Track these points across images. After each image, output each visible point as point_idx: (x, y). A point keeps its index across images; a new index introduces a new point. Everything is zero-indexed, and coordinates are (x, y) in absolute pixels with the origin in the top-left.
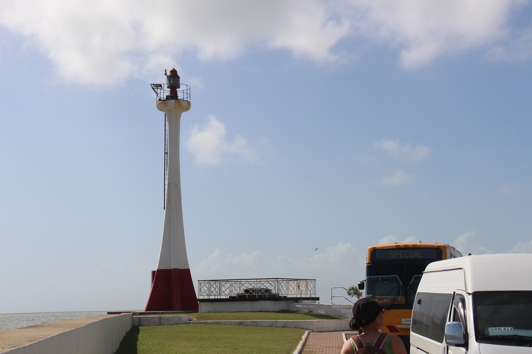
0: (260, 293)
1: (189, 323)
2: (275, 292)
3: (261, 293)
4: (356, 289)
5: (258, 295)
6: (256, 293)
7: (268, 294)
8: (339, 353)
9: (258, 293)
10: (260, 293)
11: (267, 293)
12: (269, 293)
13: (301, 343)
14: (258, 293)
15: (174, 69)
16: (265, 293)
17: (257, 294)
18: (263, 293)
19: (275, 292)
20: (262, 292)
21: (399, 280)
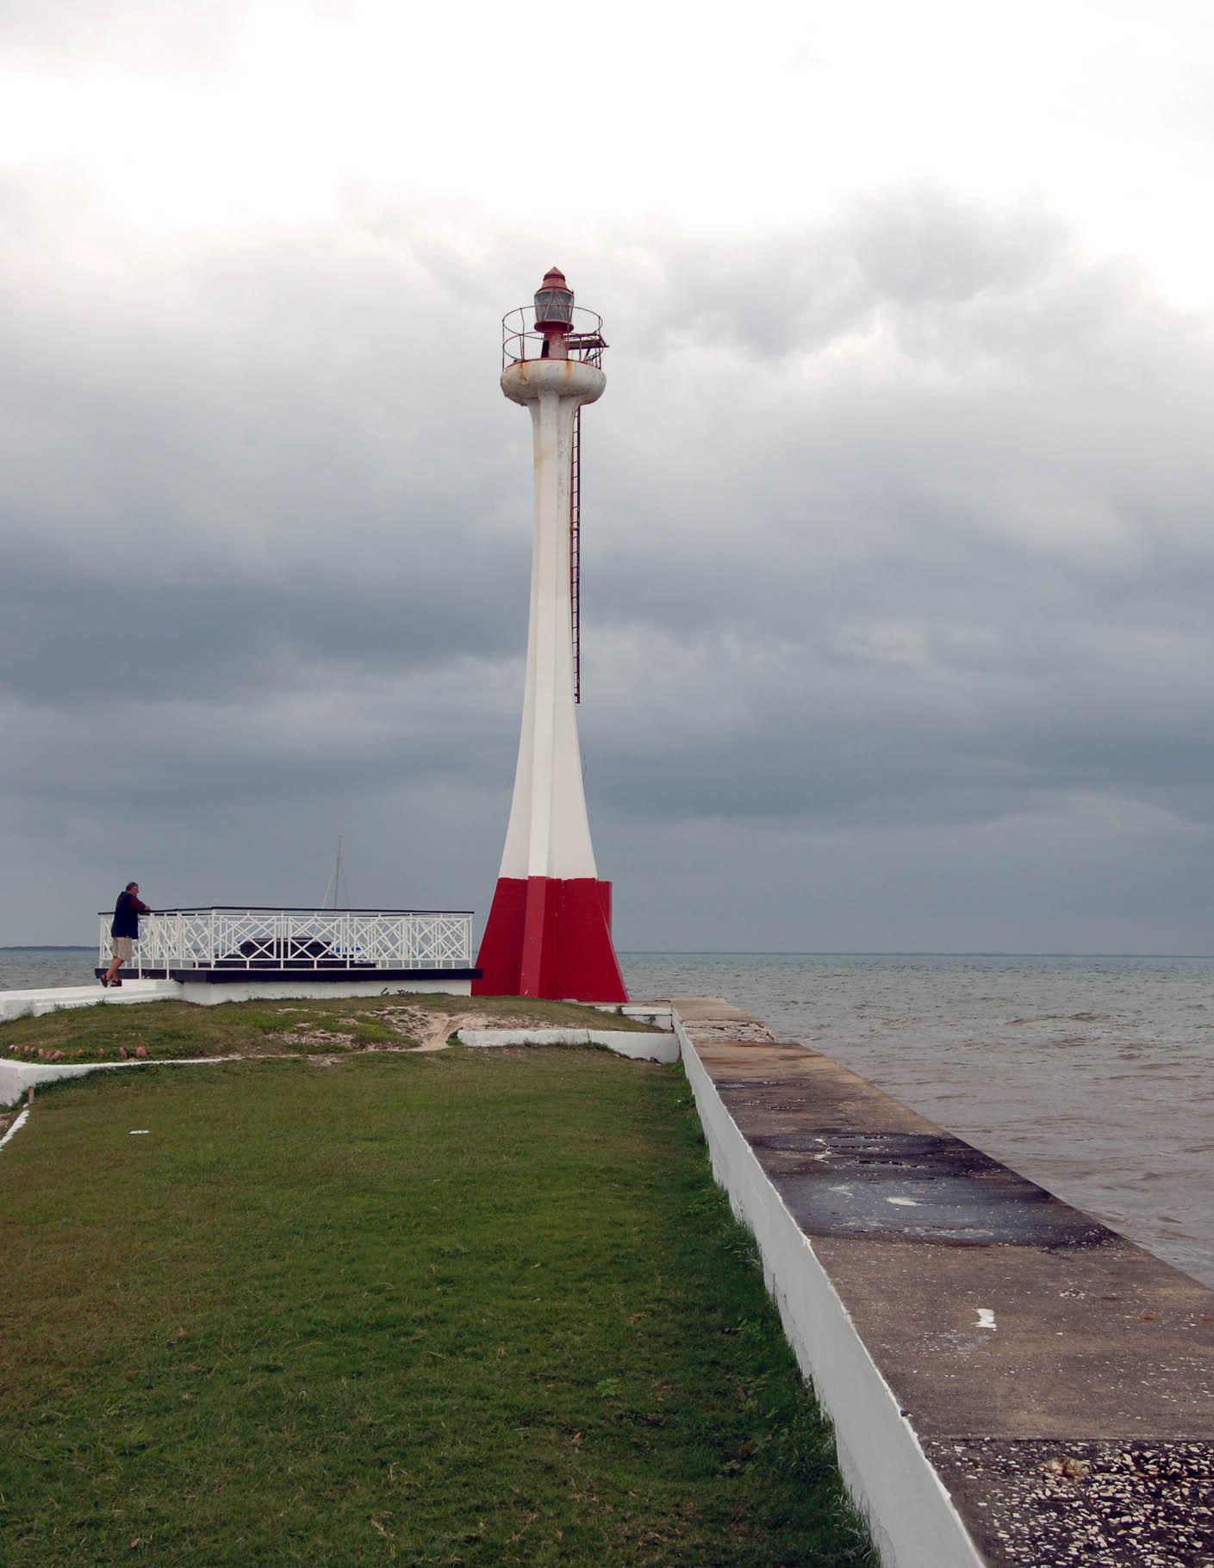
0: (292, 954)
1: (1174, 1234)
2: (439, 966)
3: (294, 955)
4: (1181, 1322)
5: (285, 961)
6: (279, 956)
7: (250, 959)
8: (7, 1055)
9: (286, 956)
10: (292, 954)
11: (248, 956)
12: (322, 954)
13: (81, 1068)
14: (286, 956)
15: (555, 268)
16: (243, 956)
17: (282, 959)
18: (302, 955)
19: (439, 966)
20: (299, 951)
21: (195, 1061)
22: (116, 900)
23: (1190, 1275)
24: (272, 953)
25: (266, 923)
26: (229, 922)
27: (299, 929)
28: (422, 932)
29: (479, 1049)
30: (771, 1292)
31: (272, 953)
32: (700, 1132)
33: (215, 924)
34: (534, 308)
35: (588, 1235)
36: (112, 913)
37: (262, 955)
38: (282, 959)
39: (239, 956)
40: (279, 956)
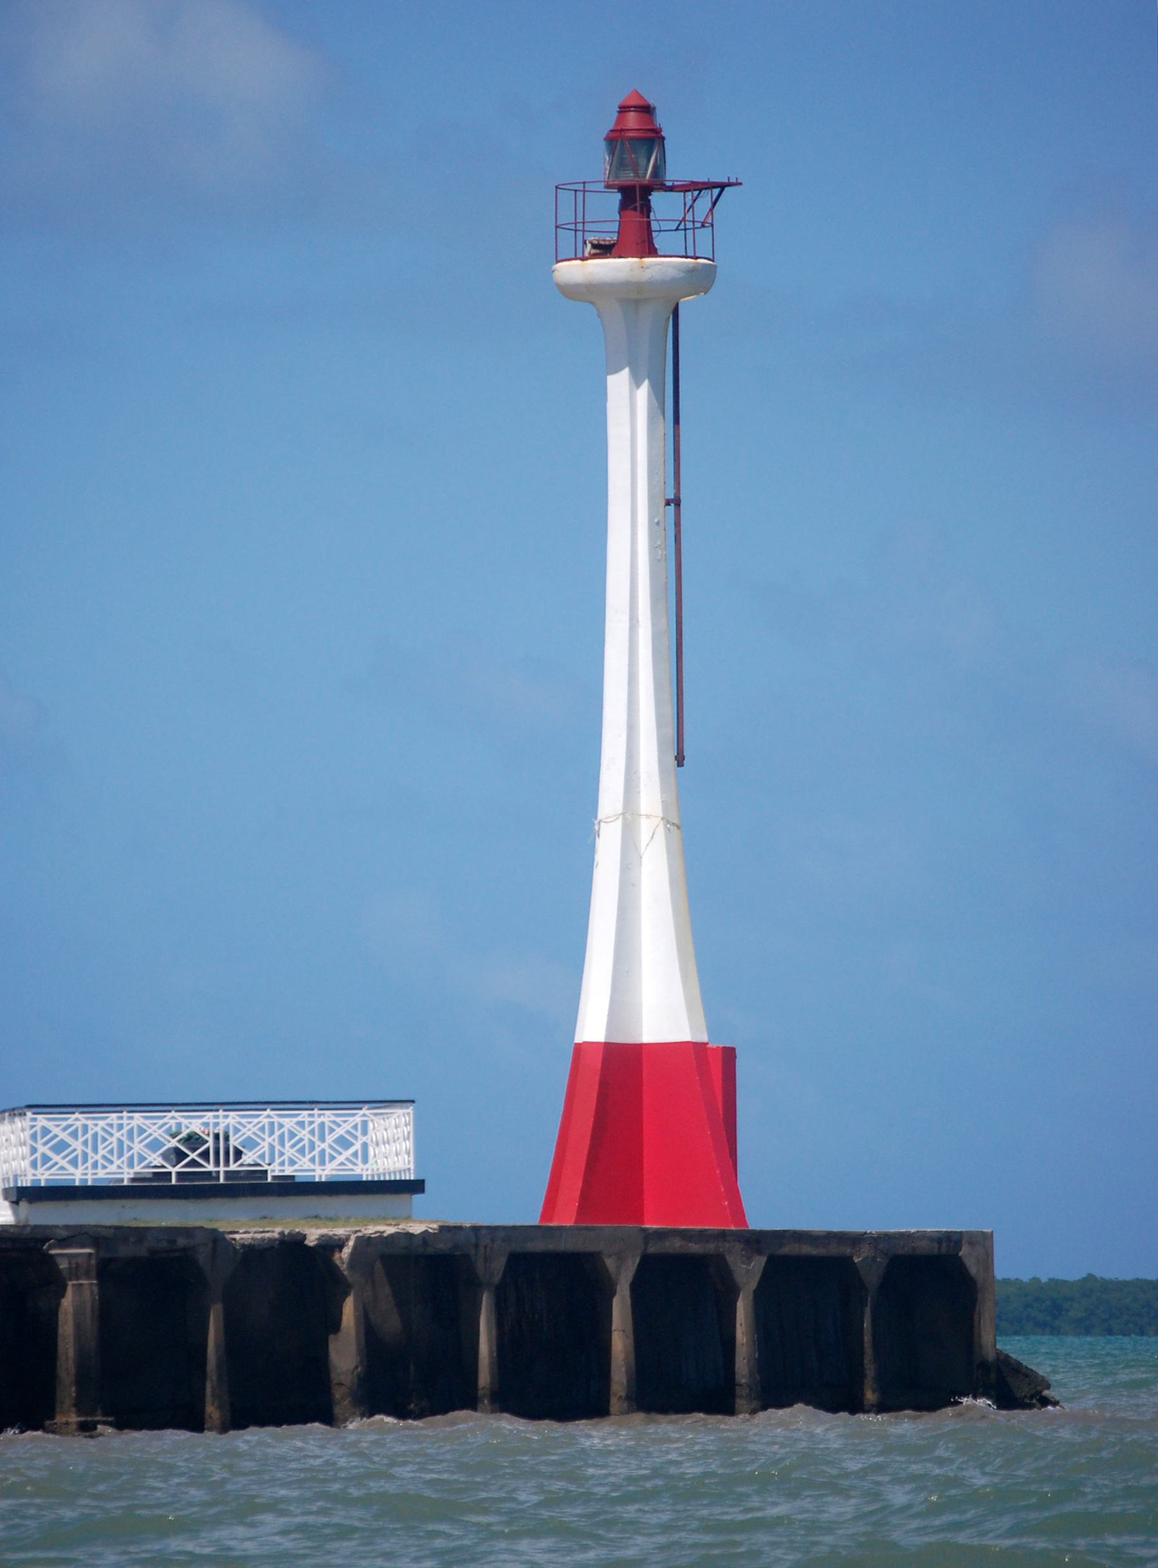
6: (217, 1163)
7: (178, 1169)
14: (227, 1163)
22: (816, 1410)
23: (1130, 1418)
24: (208, 1161)
25: (64, 1124)
26: (312, 1167)
27: (255, 1129)
28: (293, 1138)
29: (612, 1301)
30: (316, 1242)
31: (208, 1161)
32: (172, 1150)
33: (128, 1124)
34: (618, 223)
35: (603, 1439)
36: (615, 232)
37: (193, 1163)
38: (222, 1169)
39: (163, 1167)
40: (217, 1163)
